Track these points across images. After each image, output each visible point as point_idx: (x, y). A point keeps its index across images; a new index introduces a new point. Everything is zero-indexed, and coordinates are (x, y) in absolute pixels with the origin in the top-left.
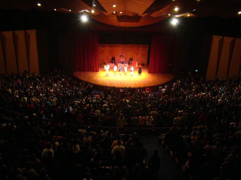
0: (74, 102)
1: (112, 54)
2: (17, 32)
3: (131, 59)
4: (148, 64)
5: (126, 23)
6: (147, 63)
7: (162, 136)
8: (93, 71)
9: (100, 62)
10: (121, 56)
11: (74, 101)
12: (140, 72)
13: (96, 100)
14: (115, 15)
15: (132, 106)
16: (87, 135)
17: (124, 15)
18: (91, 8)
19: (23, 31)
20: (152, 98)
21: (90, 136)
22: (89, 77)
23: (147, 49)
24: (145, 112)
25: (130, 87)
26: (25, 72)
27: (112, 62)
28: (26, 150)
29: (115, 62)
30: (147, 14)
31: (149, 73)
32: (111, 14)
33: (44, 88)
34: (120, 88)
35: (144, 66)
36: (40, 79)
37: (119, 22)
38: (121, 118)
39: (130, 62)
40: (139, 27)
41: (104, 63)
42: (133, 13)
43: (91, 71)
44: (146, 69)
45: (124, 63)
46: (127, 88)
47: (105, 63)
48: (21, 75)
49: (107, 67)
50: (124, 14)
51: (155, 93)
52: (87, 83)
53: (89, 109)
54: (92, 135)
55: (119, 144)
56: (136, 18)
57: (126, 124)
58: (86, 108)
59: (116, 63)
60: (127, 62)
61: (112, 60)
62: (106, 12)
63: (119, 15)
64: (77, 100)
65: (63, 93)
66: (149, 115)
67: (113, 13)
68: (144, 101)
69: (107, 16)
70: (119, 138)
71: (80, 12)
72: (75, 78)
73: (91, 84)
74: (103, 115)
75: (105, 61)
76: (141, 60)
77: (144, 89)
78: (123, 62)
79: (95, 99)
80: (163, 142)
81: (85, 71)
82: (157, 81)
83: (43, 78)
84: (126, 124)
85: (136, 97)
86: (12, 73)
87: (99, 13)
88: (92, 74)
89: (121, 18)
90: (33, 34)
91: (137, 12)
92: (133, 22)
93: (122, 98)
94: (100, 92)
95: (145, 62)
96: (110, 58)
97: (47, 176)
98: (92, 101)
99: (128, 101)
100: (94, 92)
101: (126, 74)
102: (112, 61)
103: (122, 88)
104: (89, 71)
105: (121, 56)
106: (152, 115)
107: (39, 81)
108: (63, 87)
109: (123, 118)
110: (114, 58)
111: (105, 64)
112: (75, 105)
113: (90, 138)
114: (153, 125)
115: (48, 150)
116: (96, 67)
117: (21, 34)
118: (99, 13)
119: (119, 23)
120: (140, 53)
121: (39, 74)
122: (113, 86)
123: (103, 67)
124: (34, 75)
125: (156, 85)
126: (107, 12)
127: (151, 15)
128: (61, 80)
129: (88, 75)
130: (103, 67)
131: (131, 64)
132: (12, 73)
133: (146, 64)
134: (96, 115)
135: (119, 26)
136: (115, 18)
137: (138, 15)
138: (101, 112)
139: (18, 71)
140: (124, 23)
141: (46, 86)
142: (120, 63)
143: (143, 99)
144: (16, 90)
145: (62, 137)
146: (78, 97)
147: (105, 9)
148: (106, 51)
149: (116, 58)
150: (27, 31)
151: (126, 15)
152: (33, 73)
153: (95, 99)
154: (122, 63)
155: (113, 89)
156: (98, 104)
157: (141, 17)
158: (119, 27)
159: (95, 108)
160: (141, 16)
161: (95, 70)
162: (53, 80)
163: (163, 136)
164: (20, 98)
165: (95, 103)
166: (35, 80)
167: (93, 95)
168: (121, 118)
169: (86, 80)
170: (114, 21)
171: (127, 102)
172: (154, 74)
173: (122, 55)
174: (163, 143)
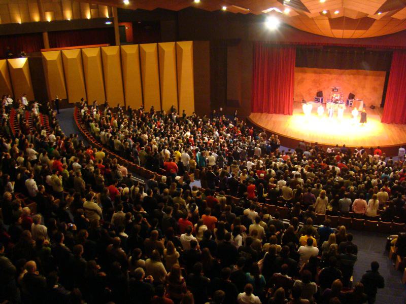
0: (245, 164)
1: (318, 85)
2: (163, 45)
3: (352, 96)
4: (382, 105)
5: (345, 31)
6: (381, 103)
7: (393, 238)
8: (283, 113)
9: (296, 99)
10: (333, 91)
11: (244, 161)
12: (363, 119)
13: (282, 163)
14: (327, 18)
15: (344, 178)
16: (258, 221)
17: (343, 17)
18: (282, 5)
19: (172, 44)
20: (383, 167)
21: (264, 223)
22: (274, 123)
23: (383, 79)
24: (367, 192)
25: (344, 146)
26: (172, 110)
27: (317, 100)
28: (157, 232)
29: (322, 100)
30: (387, 12)
31: (382, 122)
32: (319, 15)
33: (200, 137)
34: (326, 146)
35: (375, 109)
36: (195, 121)
37: (333, 30)
38: (323, 197)
39: (350, 101)
40: (367, 38)
41: (303, 100)
42: (359, 12)
43: (279, 113)
44: (379, 114)
45: (338, 103)
46: (340, 147)
47: (305, 99)
48: (165, 113)
49: (308, 107)
50: (342, 15)
51: (391, 158)
52: (269, 133)
53: (267, 177)
54: (267, 220)
55: (310, 243)
56: (365, 22)
57: (330, 208)
58: (262, 175)
59: (324, 102)
60: (343, 101)
61: (317, 96)
62: (308, 11)
63: (333, 17)
64: (250, 160)
65: (229, 146)
66: (375, 198)
67: (321, 13)
68: (367, 171)
69: (313, 19)
70: (309, 232)
71: (265, 11)
72: (250, 124)
73: (275, 134)
74: (291, 189)
75: (304, 96)
76: (371, 99)
77: (372, 150)
78: (337, 100)
79: (280, 161)
80: (393, 250)
81: (269, 112)
82: (397, 138)
83: (200, 121)
84: (330, 208)
85: (354, 164)
86: (152, 110)
87: (298, 14)
88: (280, 118)
89: (336, 22)
90: (187, 47)
91: (365, 12)
92: (357, 29)
93: (328, 163)
94: (289, 150)
95: (378, 103)
96: (315, 92)
97: (182, 278)
98: (275, 165)
99: (338, 169)
100: (279, 149)
101: (184, 111)
102: (317, 97)
103: (331, 147)
104: (275, 112)
105: (333, 91)
106: (380, 198)
107: (193, 125)
108: (230, 137)
109: (325, 197)
110: (321, 92)
111: (304, 102)
112: (246, 168)
113: (260, 227)
114: (379, 217)
115: (186, 236)
116: (283, 108)
117: (168, 47)
118: (298, 14)
119: (334, 31)
120: (369, 86)
121: (193, 113)
122: (314, 141)
123: (301, 107)
124: (184, 115)
125: (394, 144)
126: (309, 12)
127: (392, 16)
128: (227, 124)
129: (273, 119)
130: (301, 108)
131: (351, 104)
132: (152, 110)
133: (379, 106)
134: (278, 189)
135: (333, 37)
136: (327, 22)
137: (368, 16)
138: (287, 185)
139: (106, 100)
140: (341, 31)
141: (202, 134)
142: (332, 102)
143: (365, 169)
144: (156, 137)
145: (216, 219)
146: (251, 154)
147: (306, 6)
148: (305, 80)
149: (325, 94)
150: (179, 43)
151: (346, 17)
152: (95, 101)
153: (280, 161)
154: (336, 102)
155: (314, 147)
156: (284, 170)
157: (373, 20)
158: (331, 38)
159: (278, 177)
160: (374, 18)
161: (287, 112)
162: (214, 124)
163: (394, 238)
164: (160, 150)
165: (281, 168)
166: (187, 122)
167: (279, 154)
168: (323, 197)
169: (269, 127)
170: (325, 29)
171: (336, 171)
172: (391, 124)
173: (335, 88)
174: (393, 252)
